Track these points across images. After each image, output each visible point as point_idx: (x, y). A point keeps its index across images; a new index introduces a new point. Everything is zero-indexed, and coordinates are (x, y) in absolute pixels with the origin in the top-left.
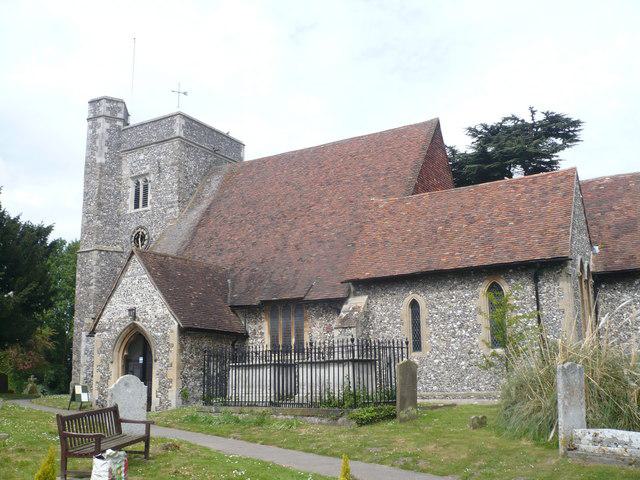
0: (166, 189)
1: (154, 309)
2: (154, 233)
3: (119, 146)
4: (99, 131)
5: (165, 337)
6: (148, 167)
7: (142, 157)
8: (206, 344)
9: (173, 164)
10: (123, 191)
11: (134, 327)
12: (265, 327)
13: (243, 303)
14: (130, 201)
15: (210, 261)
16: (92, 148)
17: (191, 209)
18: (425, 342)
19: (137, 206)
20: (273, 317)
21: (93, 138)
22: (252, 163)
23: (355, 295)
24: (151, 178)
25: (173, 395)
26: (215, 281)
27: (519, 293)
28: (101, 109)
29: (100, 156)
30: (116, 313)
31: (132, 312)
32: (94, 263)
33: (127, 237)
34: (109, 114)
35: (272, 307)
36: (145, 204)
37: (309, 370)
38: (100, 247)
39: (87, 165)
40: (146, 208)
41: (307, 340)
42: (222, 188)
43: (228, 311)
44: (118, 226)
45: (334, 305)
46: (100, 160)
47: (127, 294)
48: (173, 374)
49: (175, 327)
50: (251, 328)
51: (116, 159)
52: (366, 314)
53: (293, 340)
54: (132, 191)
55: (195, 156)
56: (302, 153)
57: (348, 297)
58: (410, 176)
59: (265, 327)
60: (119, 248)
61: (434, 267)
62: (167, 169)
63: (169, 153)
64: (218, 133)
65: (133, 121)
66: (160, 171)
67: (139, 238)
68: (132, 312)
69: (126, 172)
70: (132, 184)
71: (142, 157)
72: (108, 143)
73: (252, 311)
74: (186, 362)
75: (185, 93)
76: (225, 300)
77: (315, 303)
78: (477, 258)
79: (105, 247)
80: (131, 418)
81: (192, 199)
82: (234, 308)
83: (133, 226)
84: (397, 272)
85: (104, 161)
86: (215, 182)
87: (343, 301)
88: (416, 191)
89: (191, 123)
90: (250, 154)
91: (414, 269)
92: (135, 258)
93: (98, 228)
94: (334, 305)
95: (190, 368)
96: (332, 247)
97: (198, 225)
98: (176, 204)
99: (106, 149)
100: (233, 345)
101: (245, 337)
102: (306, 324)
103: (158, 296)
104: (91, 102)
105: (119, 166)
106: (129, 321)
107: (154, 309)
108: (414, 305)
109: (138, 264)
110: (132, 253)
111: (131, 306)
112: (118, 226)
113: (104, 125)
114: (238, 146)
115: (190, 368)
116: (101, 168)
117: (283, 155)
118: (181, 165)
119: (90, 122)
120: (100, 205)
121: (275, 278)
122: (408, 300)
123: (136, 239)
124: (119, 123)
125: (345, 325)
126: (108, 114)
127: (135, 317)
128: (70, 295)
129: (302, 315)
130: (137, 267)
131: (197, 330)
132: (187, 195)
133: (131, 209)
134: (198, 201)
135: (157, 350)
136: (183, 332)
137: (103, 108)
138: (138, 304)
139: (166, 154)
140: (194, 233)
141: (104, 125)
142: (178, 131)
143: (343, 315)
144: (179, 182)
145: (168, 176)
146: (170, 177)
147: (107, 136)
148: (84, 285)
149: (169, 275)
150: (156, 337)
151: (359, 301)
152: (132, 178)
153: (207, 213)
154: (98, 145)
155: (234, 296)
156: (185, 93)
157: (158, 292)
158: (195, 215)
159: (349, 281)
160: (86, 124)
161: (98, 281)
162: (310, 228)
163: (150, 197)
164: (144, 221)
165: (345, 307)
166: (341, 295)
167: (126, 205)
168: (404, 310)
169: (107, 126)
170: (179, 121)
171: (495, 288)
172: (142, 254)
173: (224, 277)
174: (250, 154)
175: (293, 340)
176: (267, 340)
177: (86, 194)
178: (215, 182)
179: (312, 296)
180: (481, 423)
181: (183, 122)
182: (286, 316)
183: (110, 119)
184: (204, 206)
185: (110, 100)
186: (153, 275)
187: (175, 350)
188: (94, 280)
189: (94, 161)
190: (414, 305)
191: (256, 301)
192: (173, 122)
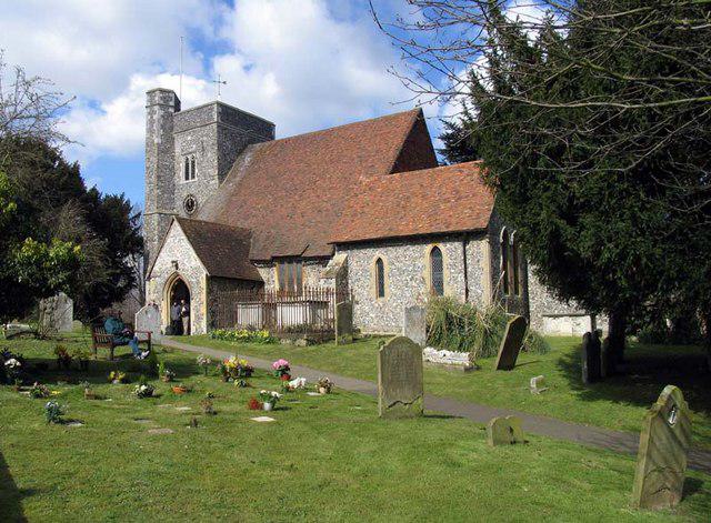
2: (201, 200)
4: (155, 117)
5: (198, 282)
7: (189, 138)
14: (182, 173)
15: (239, 225)
16: (150, 131)
18: (386, 290)
19: (187, 178)
21: (151, 122)
22: (287, 141)
24: (198, 155)
25: (204, 324)
27: (449, 250)
28: (157, 98)
36: (193, 177)
45: (323, 260)
48: (204, 310)
54: (182, 165)
58: (391, 155)
61: (393, 234)
63: (210, 135)
65: (183, 108)
66: (203, 150)
67: (190, 205)
69: (178, 150)
70: (183, 159)
71: (189, 138)
72: (162, 127)
73: (269, 263)
78: (423, 228)
80: (469, 253)
84: (368, 237)
88: (395, 170)
89: (220, 105)
91: (379, 235)
92: (176, 223)
108: (379, 261)
109: (179, 228)
111: (174, 259)
117: (301, 136)
120: (159, 177)
122: (375, 259)
126: (162, 102)
133: (183, 181)
135: (194, 291)
136: (210, 279)
139: (207, 135)
143: (328, 268)
145: (209, 155)
151: (340, 257)
164: (193, 191)
168: (373, 266)
169: (162, 112)
176: (277, 287)
179: (308, 254)
180: (195, 423)
185: (162, 91)
190: (379, 261)
191: (268, 258)
192: (212, 109)
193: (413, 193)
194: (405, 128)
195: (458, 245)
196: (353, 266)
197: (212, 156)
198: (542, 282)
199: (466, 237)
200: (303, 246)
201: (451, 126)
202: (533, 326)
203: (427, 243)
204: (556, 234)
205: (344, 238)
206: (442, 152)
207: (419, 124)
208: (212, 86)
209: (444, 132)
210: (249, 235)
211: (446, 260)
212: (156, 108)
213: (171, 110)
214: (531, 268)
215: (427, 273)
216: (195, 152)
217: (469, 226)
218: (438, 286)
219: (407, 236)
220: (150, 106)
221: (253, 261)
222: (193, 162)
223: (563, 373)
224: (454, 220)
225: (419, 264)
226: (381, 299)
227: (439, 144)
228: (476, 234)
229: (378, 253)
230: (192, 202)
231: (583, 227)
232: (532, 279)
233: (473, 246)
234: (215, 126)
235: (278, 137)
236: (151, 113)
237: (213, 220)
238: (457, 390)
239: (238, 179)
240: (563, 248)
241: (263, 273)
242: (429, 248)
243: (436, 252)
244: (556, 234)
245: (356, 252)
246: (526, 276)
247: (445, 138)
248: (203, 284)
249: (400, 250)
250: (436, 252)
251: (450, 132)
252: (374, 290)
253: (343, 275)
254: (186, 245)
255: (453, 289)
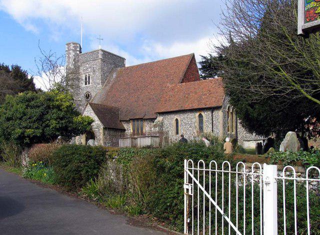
2: (93, 94)
15: (113, 105)
19: (86, 84)
27: (206, 115)
36: (89, 83)
45: (152, 120)
54: (84, 78)
58: (181, 75)
61: (183, 109)
63: (98, 64)
67: (88, 96)
73: (127, 121)
84: (172, 110)
89: (103, 51)
91: (177, 109)
108: (177, 120)
117: (139, 65)
122: (175, 119)
126: (74, 49)
133: (84, 85)
136: (105, 129)
151: (160, 118)
164: (89, 90)
168: (174, 122)
176: (132, 131)
179: (146, 117)
190: (177, 120)
193: (191, 92)
194: (187, 62)
195: (209, 113)
196: (166, 122)
197: (98, 74)
198: (243, 126)
199: (212, 109)
200: (143, 115)
201: (205, 58)
202: (239, 143)
203: (197, 112)
204: (247, 111)
205: (163, 110)
206: (200, 69)
207: (193, 58)
209: (201, 61)
210: (118, 110)
211: (205, 119)
212: (71, 51)
213: (78, 52)
214: (239, 121)
215: (197, 124)
217: (214, 105)
218: (201, 128)
219: (198, 109)
221: (121, 121)
222: (89, 77)
224: (208, 103)
225: (194, 120)
226: (177, 135)
227: (199, 66)
228: (218, 108)
229: (178, 117)
230: (89, 95)
231: (255, 108)
232: (239, 126)
233: (216, 113)
234: (100, 60)
235: (126, 66)
237: (100, 103)
238: (253, 101)
239: (110, 84)
240: (249, 115)
241: (125, 126)
242: (197, 114)
243: (200, 116)
244: (247, 111)
245: (167, 116)
246: (237, 125)
247: (201, 63)
248: (101, 131)
249: (186, 115)
250: (200, 116)
251: (204, 60)
253: (161, 125)
255: (207, 129)
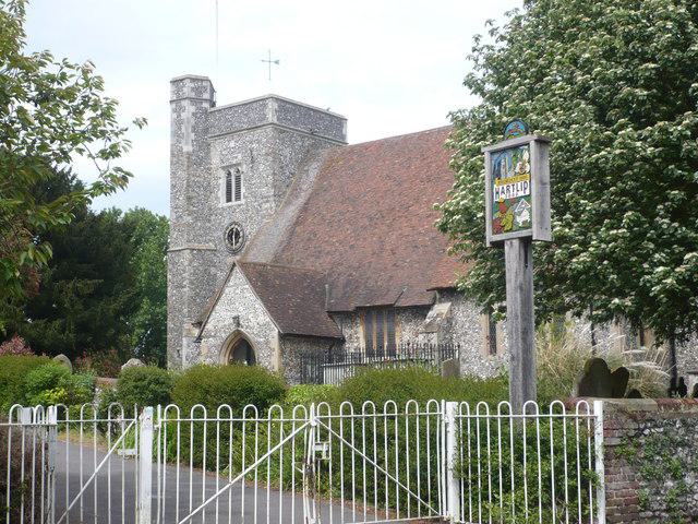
0: (259, 181)
1: (256, 317)
2: (249, 230)
3: (206, 131)
4: (184, 115)
5: (267, 343)
6: (240, 156)
8: (304, 348)
9: (267, 154)
10: (213, 182)
11: (239, 332)
12: (360, 331)
13: (339, 309)
14: (222, 193)
15: (308, 265)
16: (177, 135)
17: (288, 203)
19: (229, 200)
20: (368, 322)
21: (178, 123)
22: (365, 147)
23: (440, 302)
24: (244, 168)
26: (314, 286)
28: (185, 90)
29: (187, 143)
30: (221, 320)
31: (236, 319)
32: (186, 263)
33: (220, 234)
34: (193, 93)
35: (368, 313)
36: (238, 198)
37: (287, 504)
38: (192, 245)
39: (173, 154)
40: (239, 202)
41: (398, 341)
42: (321, 177)
43: (324, 316)
44: (209, 221)
46: (187, 148)
47: (231, 302)
49: (275, 333)
50: (347, 332)
51: (204, 146)
52: (450, 320)
53: (386, 344)
54: (223, 182)
55: (290, 141)
56: (406, 139)
57: (434, 304)
59: (360, 331)
60: (212, 246)
62: (261, 159)
63: (262, 141)
64: (316, 111)
66: (253, 162)
67: (233, 235)
68: (236, 319)
69: (215, 160)
70: (222, 174)
71: (232, 144)
73: (349, 316)
74: (287, 364)
75: (277, 62)
76: (323, 305)
77: (405, 309)
79: (196, 245)
81: (289, 191)
82: (331, 314)
83: (226, 222)
85: (191, 149)
86: (313, 171)
87: (428, 308)
89: (285, 106)
90: (355, 135)
92: (237, 269)
93: (189, 225)
94: (420, 311)
95: (290, 370)
96: (425, 253)
97: (297, 223)
98: (272, 199)
99: (193, 136)
100: (330, 349)
101: (342, 341)
102: (397, 328)
103: (259, 305)
104: (175, 82)
105: (208, 153)
106: (233, 328)
107: (256, 317)
109: (240, 275)
110: (234, 265)
111: (235, 314)
112: (209, 221)
113: (190, 109)
114: (338, 122)
115: (290, 370)
116: (188, 158)
117: (386, 140)
118: (275, 155)
119: (174, 105)
120: (189, 198)
121: (371, 283)
123: (230, 236)
124: (206, 105)
125: (428, 331)
126: (193, 95)
127: (238, 324)
128: (159, 296)
129: (393, 321)
130: (238, 277)
131: (298, 336)
132: (284, 188)
133: (223, 203)
134: (295, 194)
136: (283, 337)
137: (187, 89)
138: (242, 312)
140: (292, 233)
141: (190, 109)
142: (271, 117)
143: (428, 320)
144: (275, 174)
145: (261, 168)
146: (264, 167)
147: (193, 121)
148: (177, 287)
149: (267, 283)
150: (259, 343)
151: (442, 308)
152: (223, 168)
153: (305, 209)
154: (183, 130)
155: (332, 302)
156: (277, 62)
157: (259, 301)
158: (292, 211)
159: (434, 289)
160: (168, 108)
161: (192, 283)
162: (407, 231)
163: (243, 190)
164: (238, 217)
165: (430, 313)
166: (427, 302)
167: (217, 198)
169: (192, 109)
170: (272, 105)
171: (453, 368)
172: (244, 266)
173: (321, 283)
174: (355, 135)
175: (386, 344)
176: (362, 345)
177: (173, 186)
178: (313, 171)
179: (403, 303)
181: (276, 106)
182: (379, 321)
183: (195, 101)
184: (301, 200)
185: (194, 80)
186: (254, 286)
187: (276, 353)
188: (187, 281)
189: (181, 150)
191: (351, 307)
192: (265, 106)
208: (630, 404)
216: (239, 164)
220: (176, 102)
223: (51, 69)
230: (237, 234)
236: (178, 110)
248: (275, 343)
252: (484, 346)
254: (250, 294)
